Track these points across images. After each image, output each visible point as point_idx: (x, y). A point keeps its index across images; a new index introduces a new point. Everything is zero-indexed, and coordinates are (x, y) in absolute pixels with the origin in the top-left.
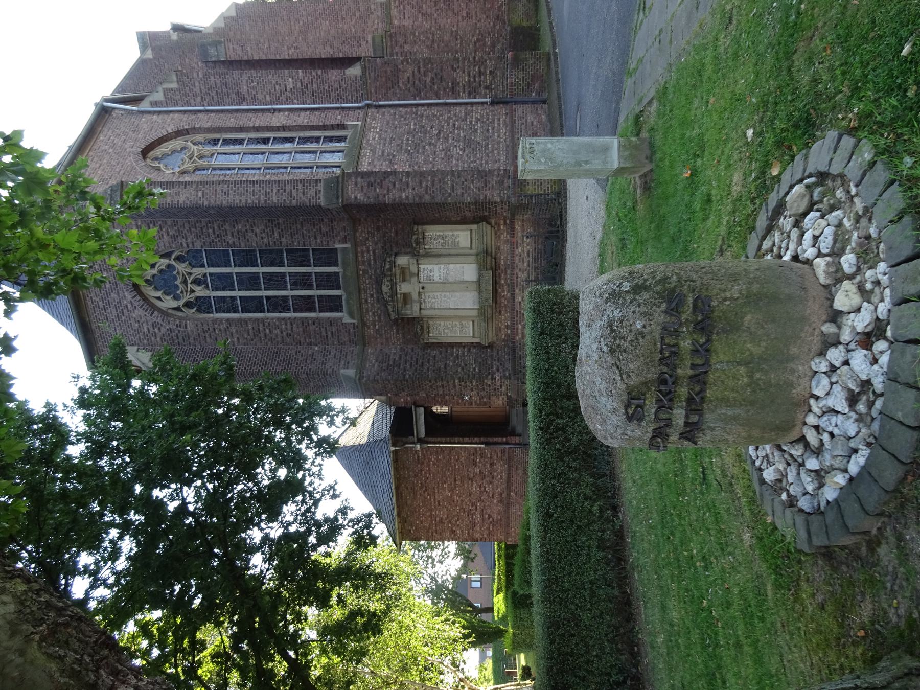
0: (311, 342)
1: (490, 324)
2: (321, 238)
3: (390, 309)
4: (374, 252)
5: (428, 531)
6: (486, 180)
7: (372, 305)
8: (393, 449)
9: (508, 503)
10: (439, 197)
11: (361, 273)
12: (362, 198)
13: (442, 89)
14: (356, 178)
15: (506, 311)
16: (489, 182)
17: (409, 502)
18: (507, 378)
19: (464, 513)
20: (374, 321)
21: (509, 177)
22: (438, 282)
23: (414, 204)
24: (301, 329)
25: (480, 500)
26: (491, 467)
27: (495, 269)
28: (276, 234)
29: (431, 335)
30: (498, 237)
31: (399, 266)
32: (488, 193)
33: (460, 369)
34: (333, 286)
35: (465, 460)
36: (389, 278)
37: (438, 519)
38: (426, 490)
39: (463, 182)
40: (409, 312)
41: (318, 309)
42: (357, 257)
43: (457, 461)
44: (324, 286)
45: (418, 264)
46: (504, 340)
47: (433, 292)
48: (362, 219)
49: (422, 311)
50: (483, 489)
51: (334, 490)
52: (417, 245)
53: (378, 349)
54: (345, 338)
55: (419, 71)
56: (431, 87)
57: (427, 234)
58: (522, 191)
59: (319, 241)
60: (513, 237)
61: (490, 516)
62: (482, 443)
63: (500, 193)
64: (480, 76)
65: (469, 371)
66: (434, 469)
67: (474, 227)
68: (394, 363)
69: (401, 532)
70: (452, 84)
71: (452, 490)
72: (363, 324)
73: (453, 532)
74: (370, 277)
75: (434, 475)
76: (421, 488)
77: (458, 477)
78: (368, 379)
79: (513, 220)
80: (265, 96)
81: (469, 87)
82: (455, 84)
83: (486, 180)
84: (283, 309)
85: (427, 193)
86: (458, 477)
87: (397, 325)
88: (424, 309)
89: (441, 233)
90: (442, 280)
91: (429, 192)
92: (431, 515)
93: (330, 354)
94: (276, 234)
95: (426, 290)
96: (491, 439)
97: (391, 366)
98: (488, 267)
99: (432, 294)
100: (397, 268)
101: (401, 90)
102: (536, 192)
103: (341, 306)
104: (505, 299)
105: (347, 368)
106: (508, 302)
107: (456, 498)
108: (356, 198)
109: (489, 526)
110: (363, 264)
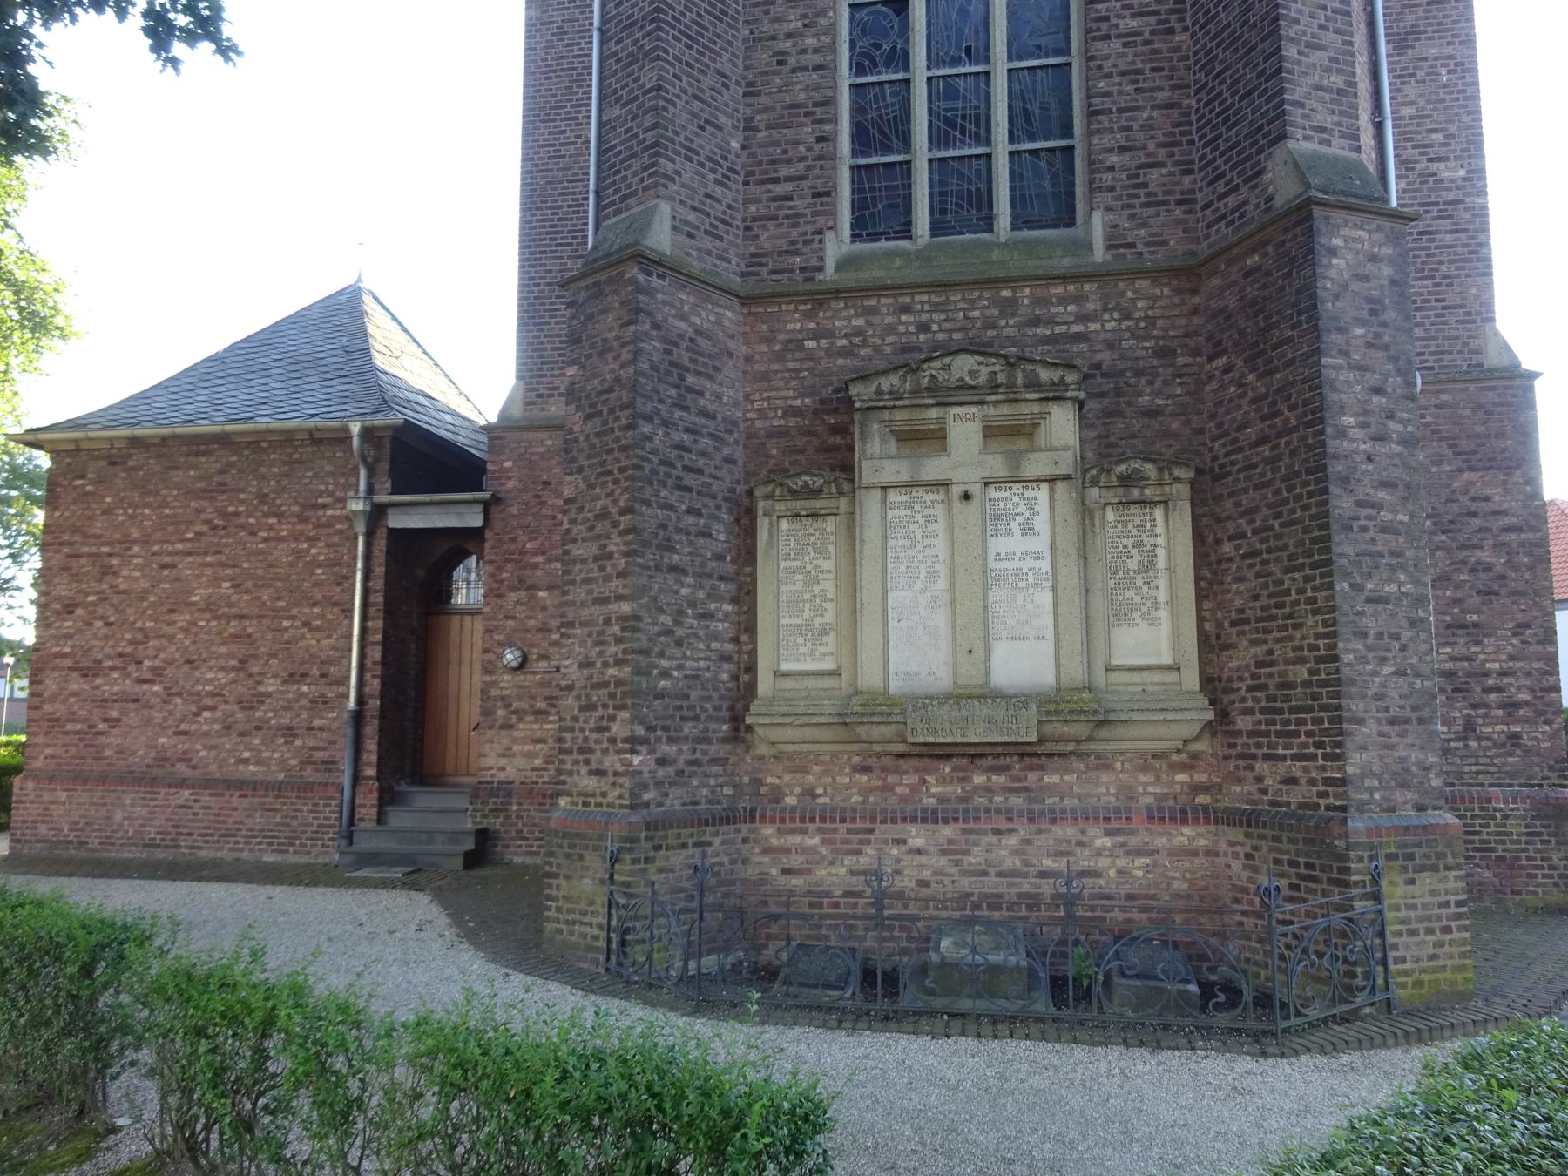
0: (756, 129)
1: (824, 734)
2: (1124, 168)
3: (886, 383)
4: (1080, 338)
5: (75, 530)
6: (1407, 721)
7: (892, 329)
8: (355, 428)
9: (154, 782)
10: (1349, 550)
11: (1006, 293)
12: (1332, 273)
13: (1459, 594)
14: (1391, 261)
15: (867, 791)
16: (1402, 735)
17: (177, 476)
18: (633, 795)
19: (130, 643)
20: (830, 334)
21: (1421, 808)
22: (985, 550)
23: (1324, 455)
24: (802, 97)
25: (170, 695)
26: (280, 728)
27: (1034, 755)
28: (1134, 23)
29: (784, 524)
30: (1149, 761)
31: (1045, 415)
32: (1369, 730)
33: (667, 620)
34: (943, 212)
35: (307, 649)
36: (1002, 378)
37: (115, 561)
38: (215, 528)
39: (1397, 637)
40: (874, 446)
41: (863, 161)
42: (1064, 278)
43: (305, 624)
44: (943, 183)
45: (1052, 480)
46: (758, 782)
47: (951, 530)
48: (1197, 300)
49: (877, 494)
50: (208, 701)
51: (190, 37)
52: (1121, 478)
53: (731, 344)
54: (768, 238)
55: (1509, 529)
56: (1464, 563)
57: (1159, 513)
58: (1390, 857)
59: (1114, 159)
60: (1151, 818)
61: (114, 723)
62: (361, 700)
63: (1374, 775)
64: (1503, 706)
65: (661, 655)
66: (282, 553)
67: (1191, 679)
68: (690, 390)
69: (78, 450)
70: (1476, 625)
71: (209, 607)
72: (822, 298)
73: (69, 608)
74: (990, 324)
75: (262, 552)
76: (224, 514)
77: (250, 627)
78: (639, 290)
79: (1208, 816)
80: (1412, 103)
81: (1469, 674)
82: (1476, 632)
83: (1407, 721)
84: (862, 54)
85: (1359, 504)
86: (250, 627)
87: (816, 412)
88: (884, 501)
89: (1161, 563)
90: (992, 564)
91: (1364, 512)
92: (128, 542)
93: (717, 182)
94: (1134, 23)
95: (957, 505)
96: (371, 730)
97: (682, 377)
98: (1049, 729)
99: (939, 527)
100: (1036, 408)
101: (1452, 476)
102: (1389, 915)
103: (874, 237)
104: (913, 788)
105: (675, 228)
106: (903, 799)
107: (182, 619)
108: (1333, 252)
109: (82, 721)
110: (1038, 301)
